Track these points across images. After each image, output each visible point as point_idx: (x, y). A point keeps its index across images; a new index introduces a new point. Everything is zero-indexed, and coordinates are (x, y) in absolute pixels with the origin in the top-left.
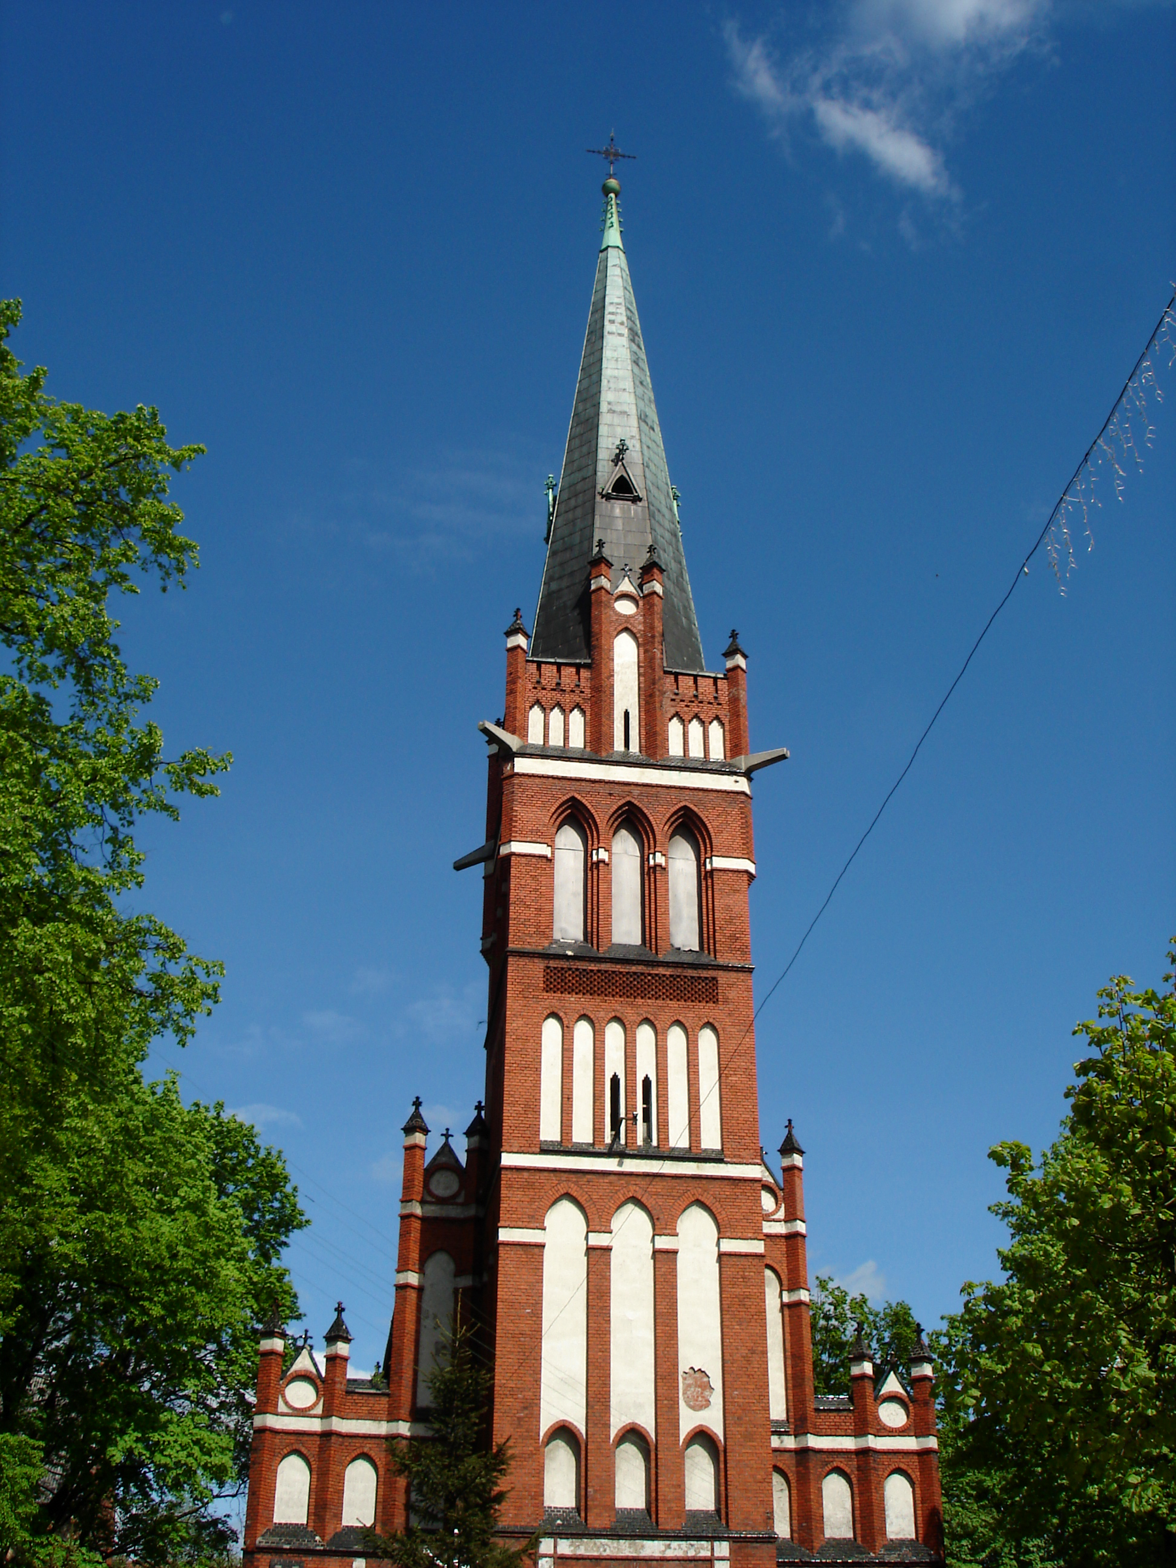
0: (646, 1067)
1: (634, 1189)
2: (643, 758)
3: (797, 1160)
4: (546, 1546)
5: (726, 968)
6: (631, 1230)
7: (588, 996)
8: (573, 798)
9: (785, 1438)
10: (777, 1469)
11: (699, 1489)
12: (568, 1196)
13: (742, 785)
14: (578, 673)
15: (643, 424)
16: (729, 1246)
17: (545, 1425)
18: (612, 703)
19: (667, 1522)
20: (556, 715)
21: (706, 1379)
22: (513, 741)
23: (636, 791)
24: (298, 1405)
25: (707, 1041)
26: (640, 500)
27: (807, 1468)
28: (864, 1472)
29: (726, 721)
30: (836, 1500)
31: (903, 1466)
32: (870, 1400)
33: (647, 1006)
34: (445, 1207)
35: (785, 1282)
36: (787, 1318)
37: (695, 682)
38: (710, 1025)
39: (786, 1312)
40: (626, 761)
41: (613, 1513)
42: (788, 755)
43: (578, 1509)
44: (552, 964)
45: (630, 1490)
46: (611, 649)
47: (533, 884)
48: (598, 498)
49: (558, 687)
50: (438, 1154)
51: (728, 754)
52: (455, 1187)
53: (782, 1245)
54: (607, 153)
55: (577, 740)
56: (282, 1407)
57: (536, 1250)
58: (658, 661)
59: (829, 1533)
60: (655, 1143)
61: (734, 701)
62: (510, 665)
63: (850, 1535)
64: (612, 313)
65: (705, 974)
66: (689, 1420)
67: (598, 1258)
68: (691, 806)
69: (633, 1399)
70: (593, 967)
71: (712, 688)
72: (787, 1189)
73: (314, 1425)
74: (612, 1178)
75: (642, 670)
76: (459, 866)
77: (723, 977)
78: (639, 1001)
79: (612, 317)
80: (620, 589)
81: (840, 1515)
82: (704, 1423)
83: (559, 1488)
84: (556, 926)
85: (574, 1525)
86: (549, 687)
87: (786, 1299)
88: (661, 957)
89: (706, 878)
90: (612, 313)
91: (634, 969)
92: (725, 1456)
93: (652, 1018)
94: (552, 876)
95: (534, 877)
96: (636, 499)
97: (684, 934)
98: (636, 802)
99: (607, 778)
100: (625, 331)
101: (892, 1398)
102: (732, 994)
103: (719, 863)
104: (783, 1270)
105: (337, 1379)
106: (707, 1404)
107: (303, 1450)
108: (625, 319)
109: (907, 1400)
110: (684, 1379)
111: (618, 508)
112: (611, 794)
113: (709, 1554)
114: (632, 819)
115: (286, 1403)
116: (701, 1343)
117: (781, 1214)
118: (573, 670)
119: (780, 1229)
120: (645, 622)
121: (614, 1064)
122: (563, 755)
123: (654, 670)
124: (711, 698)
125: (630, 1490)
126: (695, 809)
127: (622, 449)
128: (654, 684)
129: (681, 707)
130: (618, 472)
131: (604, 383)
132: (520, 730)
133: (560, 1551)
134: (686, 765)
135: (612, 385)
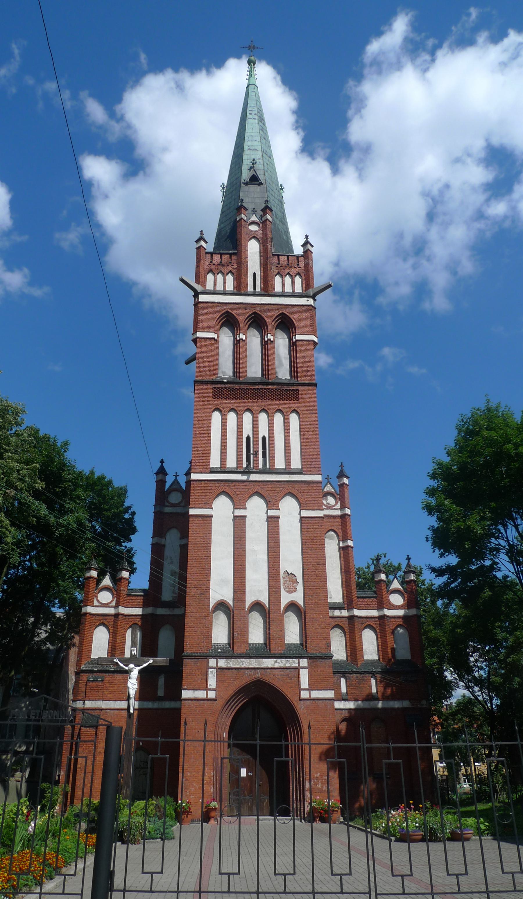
0: (263, 431)
1: (257, 488)
2: (263, 293)
3: (346, 481)
6: (256, 509)
8: (227, 312)
9: (343, 611)
11: (292, 633)
12: (224, 493)
13: (311, 302)
14: (231, 257)
15: (264, 155)
16: (305, 513)
17: (212, 603)
18: (247, 269)
19: (275, 650)
20: (220, 277)
21: (294, 578)
22: (199, 288)
23: (258, 307)
25: (294, 419)
26: (262, 184)
29: (303, 275)
32: (384, 592)
33: (264, 403)
34: (175, 508)
35: (341, 537)
36: (342, 554)
37: (288, 259)
38: (295, 411)
39: (342, 551)
40: (254, 294)
42: (332, 285)
43: (229, 644)
44: (217, 386)
45: (256, 635)
46: (247, 246)
47: (208, 351)
48: (242, 185)
50: (172, 484)
51: (304, 289)
52: (180, 499)
53: (339, 520)
54: (249, 47)
55: (230, 287)
56: (96, 603)
57: (208, 518)
58: (269, 250)
59: (366, 657)
60: (268, 467)
63: (376, 658)
64: (251, 111)
65: (292, 388)
66: (285, 598)
68: (286, 313)
69: (257, 588)
70: (237, 386)
71: (296, 261)
72: (341, 495)
73: (111, 611)
75: (262, 254)
77: (301, 389)
78: (260, 401)
79: (250, 112)
80: (251, 219)
81: (371, 648)
83: (220, 634)
84: (220, 371)
85: (228, 652)
86: (216, 264)
87: (341, 545)
88: (270, 381)
89: (293, 345)
90: (251, 111)
92: (305, 616)
93: (266, 409)
95: (208, 348)
96: (260, 184)
97: (283, 373)
98: (258, 312)
99: (244, 302)
100: (256, 117)
101: (396, 591)
102: (306, 396)
103: (299, 337)
104: (340, 531)
105: (122, 589)
106: (296, 590)
107: (106, 622)
108: (257, 112)
109: (403, 591)
110: (284, 578)
111: (253, 188)
112: (246, 309)
113: (297, 665)
114: (257, 321)
115: (98, 601)
116: (292, 560)
117: (338, 506)
120: (263, 233)
121: (247, 430)
122: (224, 293)
123: (267, 253)
124: (295, 265)
125: (256, 635)
126: (288, 314)
127: (254, 162)
128: (267, 259)
129: (281, 270)
130: (252, 173)
131: (246, 138)
132: (204, 284)
135: (250, 139)
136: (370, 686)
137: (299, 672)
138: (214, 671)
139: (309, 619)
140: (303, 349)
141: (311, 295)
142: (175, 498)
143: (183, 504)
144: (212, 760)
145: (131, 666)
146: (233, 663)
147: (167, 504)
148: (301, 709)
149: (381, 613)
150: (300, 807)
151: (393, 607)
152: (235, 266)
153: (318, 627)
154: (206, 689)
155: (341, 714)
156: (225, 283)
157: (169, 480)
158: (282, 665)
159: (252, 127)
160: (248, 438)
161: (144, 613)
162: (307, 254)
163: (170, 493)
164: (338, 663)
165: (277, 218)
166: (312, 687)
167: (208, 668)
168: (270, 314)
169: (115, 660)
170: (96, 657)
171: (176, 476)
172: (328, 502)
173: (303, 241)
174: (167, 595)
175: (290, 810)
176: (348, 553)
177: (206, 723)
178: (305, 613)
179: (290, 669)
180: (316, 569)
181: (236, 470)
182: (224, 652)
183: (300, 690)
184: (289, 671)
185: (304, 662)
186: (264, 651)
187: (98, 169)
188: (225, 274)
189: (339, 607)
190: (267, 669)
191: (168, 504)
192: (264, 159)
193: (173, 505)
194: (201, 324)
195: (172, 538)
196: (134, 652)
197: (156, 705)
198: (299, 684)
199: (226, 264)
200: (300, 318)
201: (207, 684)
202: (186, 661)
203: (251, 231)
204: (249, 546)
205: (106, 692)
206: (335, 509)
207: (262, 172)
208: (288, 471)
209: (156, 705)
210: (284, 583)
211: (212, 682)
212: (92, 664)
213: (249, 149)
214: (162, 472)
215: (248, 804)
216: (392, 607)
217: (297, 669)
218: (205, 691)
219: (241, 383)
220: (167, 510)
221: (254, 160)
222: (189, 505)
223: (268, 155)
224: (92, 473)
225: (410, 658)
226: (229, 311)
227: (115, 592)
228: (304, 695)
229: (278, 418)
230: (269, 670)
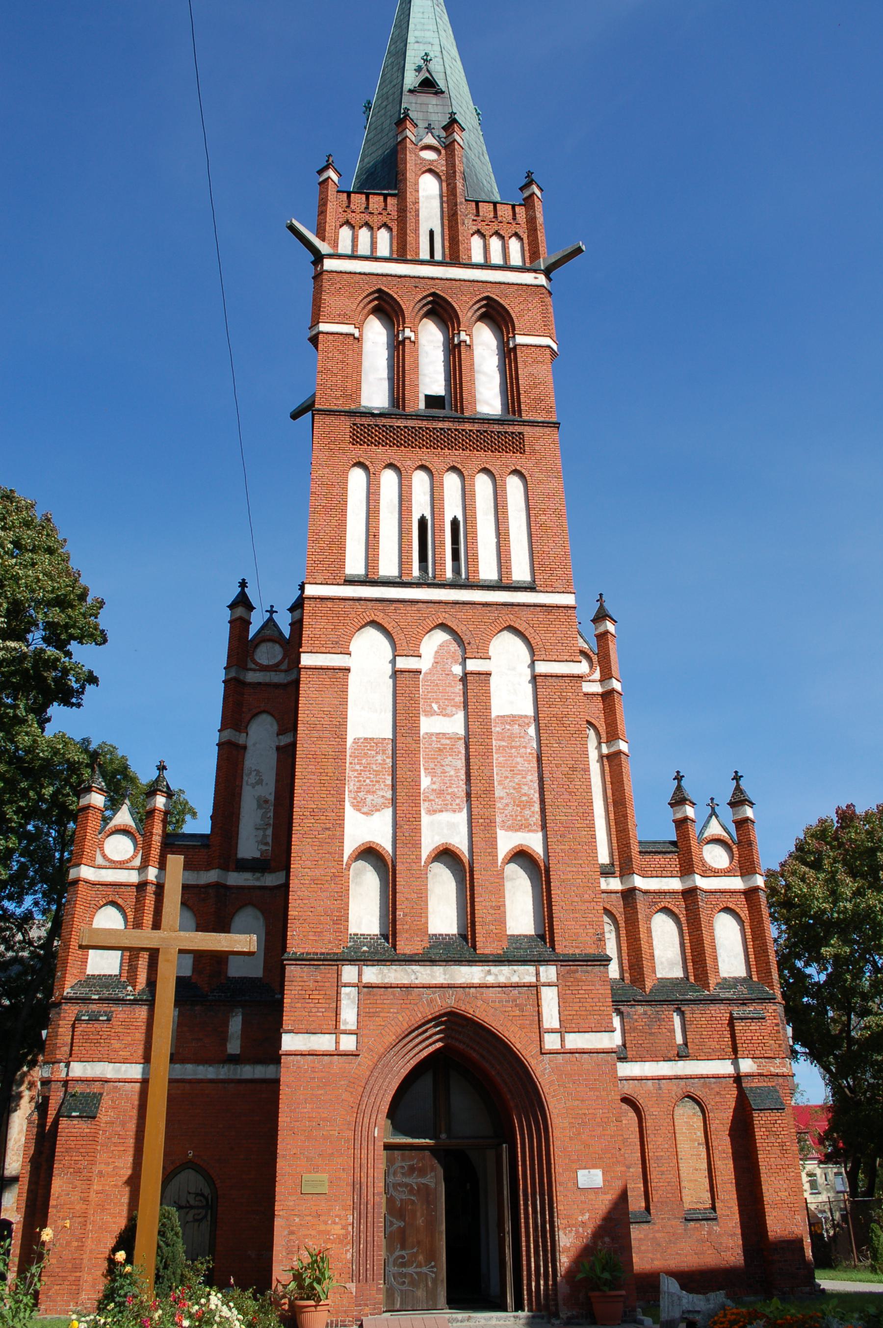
0: (453, 509)
3: (610, 627)
5: (533, 424)
9: (611, 880)
10: (607, 912)
11: (520, 916)
12: (374, 623)
14: (385, 201)
16: (542, 668)
17: (350, 847)
19: (485, 947)
20: (364, 234)
22: (324, 248)
24: (116, 858)
25: (514, 487)
27: (635, 908)
28: (691, 912)
30: (664, 941)
31: (731, 905)
32: (693, 843)
39: (605, 760)
40: (432, 262)
41: (426, 938)
42: (584, 248)
43: (385, 936)
44: (358, 421)
47: (340, 357)
50: (263, 628)
51: (528, 261)
52: (279, 657)
55: (384, 249)
56: (100, 860)
61: (531, 221)
62: (321, 193)
65: (510, 429)
68: (494, 296)
71: (511, 213)
75: (445, 199)
77: (527, 430)
82: (524, 843)
85: (387, 948)
86: (358, 211)
87: (605, 750)
88: (466, 414)
91: (440, 425)
93: (459, 466)
94: (360, 354)
103: (520, 339)
104: (602, 729)
107: (120, 901)
112: (416, 287)
113: (534, 980)
117: (597, 675)
118: (381, 198)
119: (597, 688)
121: (421, 506)
123: (455, 196)
125: (443, 919)
126: (498, 299)
127: (426, 59)
130: (424, 75)
134: (487, 266)
135: (418, 27)
137: (538, 993)
138: (354, 991)
139: (558, 883)
140: (530, 360)
141: (542, 268)
142: (267, 655)
143: (284, 666)
144: (350, 1188)
148: (543, 1072)
149: (689, 885)
151: (710, 872)
152: (395, 214)
153: (576, 899)
154: (336, 1030)
157: (257, 621)
158: (502, 980)
159: (421, 10)
163: (257, 646)
167: (339, 985)
168: (464, 298)
171: (272, 611)
174: (249, 846)
176: (620, 765)
178: (547, 870)
179: (518, 987)
181: (398, 580)
182: (376, 953)
183: (541, 1032)
184: (515, 992)
185: (549, 973)
186: (464, 947)
188: (375, 228)
189: (606, 872)
190: (470, 987)
191: (253, 666)
194: (325, 310)
195: (261, 735)
197: (223, 1072)
198: (540, 1021)
199: (376, 212)
200: (522, 307)
202: (292, 971)
205: (116, 1044)
207: (442, 76)
209: (223, 1072)
211: (349, 1015)
212: (88, 986)
214: (242, 602)
215: (427, 1285)
216: (709, 873)
217: (536, 987)
218: (334, 1036)
219: (407, 417)
220: (252, 677)
221: (426, 55)
222: (301, 647)
226: (383, 288)
227: (140, 839)
228: (552, 1042)
229: (483, 485)
230: (473, 990)
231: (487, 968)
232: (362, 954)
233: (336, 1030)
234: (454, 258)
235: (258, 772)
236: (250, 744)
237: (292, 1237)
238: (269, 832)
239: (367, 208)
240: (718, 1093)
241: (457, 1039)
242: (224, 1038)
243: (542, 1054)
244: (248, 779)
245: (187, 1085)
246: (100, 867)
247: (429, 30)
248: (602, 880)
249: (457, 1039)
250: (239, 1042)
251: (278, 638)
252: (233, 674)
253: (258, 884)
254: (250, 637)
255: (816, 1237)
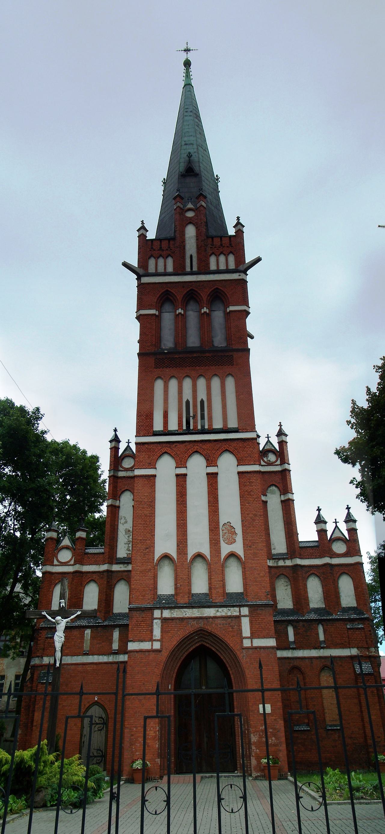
0: (202, 395)
4: (157, 613)
6: (197, 466)
7: (174, 368)
8: (167, 290)
11: (234, 582)
15: (200, 148)
17: (157, 556)
21: (233, 530)
40: (192, 273)
45: (200, 584)
49: (161, 249)
56: (56, 562)
57: (152, 478)
65: (227, 354)
66: (225, 549)
67: (181, 479)
69: (199, 540)
73: (70, 569)
74: (187, 444)
76: (258, 260)
78: (198, 368)
83: (166, 585)
87: (283, 499)
91: (181, 356)
106: (235, 541)
115: (58, 560)
116: (231, 510)
117: (278, 462)
121: (187, 395)
122: (165, 274)
125: (200, 584)
133: (164, 616)
134: (218, 272)
136: (318, 634)
138: (159, 621)
145: (59, 618)
146: (177, 614)
147: (263, 463)
148: (243, 657)
150: (184, 644)
154: (151, 640)
155: (120, 489)
156: (165, 266)
157: (122, 447)
159: (188, 123)
160: (202, 402)
161: (162, 236)
162: (240, 232)
164: (284, 612)
165: (211, 204)
166: (253, 636)
169: (43, 613)
170: (249, 346)
171: (129, 443)
172: (269, 459)
173: (111, 435)
175: (233, 772)
177: (260, 666)
180: (254, 520)
181: (176, 432)
185: (245, 611)
187: (353, 421)
191: (121, 469)
192: (200, 152)
193: (127, 470)
196: (63, 604)
197: (111, 659)
201: (152, 635)
203: (187, 217)
204: (177, 436)
206: (68, 565)
208: (166, 432)
209: (111, 659)
210: (223, 535)
211: (157, 632)
213: (186, 144)
214: (116, 440)
220: (121, 474)
223: (204, 148)
224: (346, 456)
225: (355, 605)
231: (217, 609)
232: (170, 603)
233: (253, 636)
234: (204, 269)
235: (125, 518)
236: (121, 505)
237: (132, 737)
238: (130, 545)
239: (161, 248)
240: (341, 665)
241: (205, 642)
242: (111, 642)
243: (146, 718)
244: (121, 521)
245: (95, 666)
246: (56, 565)
247: (191, 136)
248: (268, 561)
249: (205, 642)
250: (117, 644)
251: (274, 451)
252: (112, 474)
253: (126, 569)
254: (119, 455)
255: (116, 460)
